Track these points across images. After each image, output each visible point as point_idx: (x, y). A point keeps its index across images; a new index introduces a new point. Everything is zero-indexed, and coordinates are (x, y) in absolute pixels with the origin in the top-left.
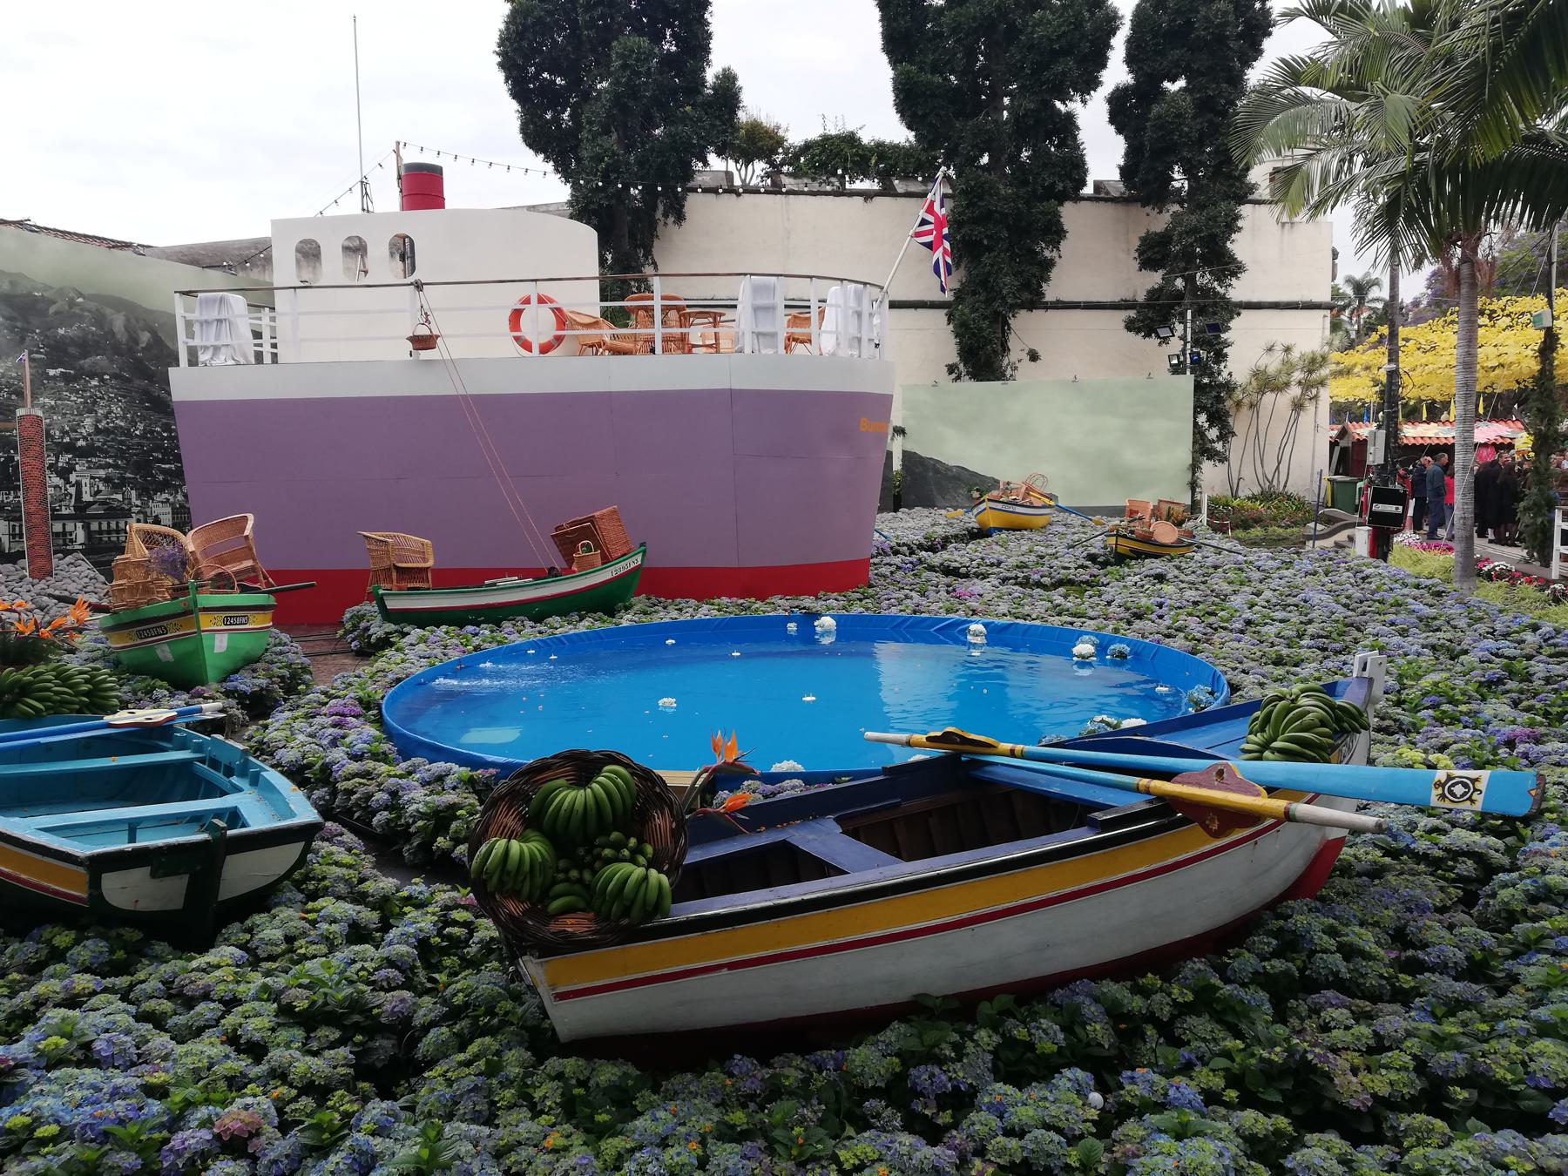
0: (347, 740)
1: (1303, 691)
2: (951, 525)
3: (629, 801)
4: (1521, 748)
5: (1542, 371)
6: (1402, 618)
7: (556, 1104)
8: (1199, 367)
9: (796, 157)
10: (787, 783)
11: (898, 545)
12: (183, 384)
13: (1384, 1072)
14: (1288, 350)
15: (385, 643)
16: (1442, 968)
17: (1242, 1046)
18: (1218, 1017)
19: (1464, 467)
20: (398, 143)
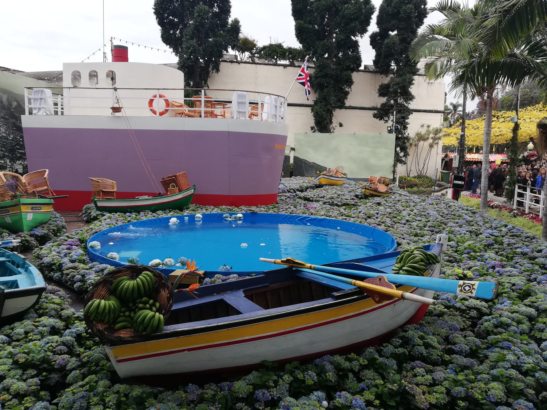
0: (71, 255)
1: (415, 249)
2: (309, 183)
3: (151, 286)
4: (497, 269)
5: (513, 137)
6: (461, 221)
7: (114, 403)
8: (397, 131)
9: (260, 51)
10: (232, 276)
11: (290, 189)
12: (26, 121)
13: (434, 394)
14: (428, 126)
15: (95, 218)
16: (460, 353)
17: (383, 383)
18: (376, 371)
19: (485, 169)
20: (112, 38)
